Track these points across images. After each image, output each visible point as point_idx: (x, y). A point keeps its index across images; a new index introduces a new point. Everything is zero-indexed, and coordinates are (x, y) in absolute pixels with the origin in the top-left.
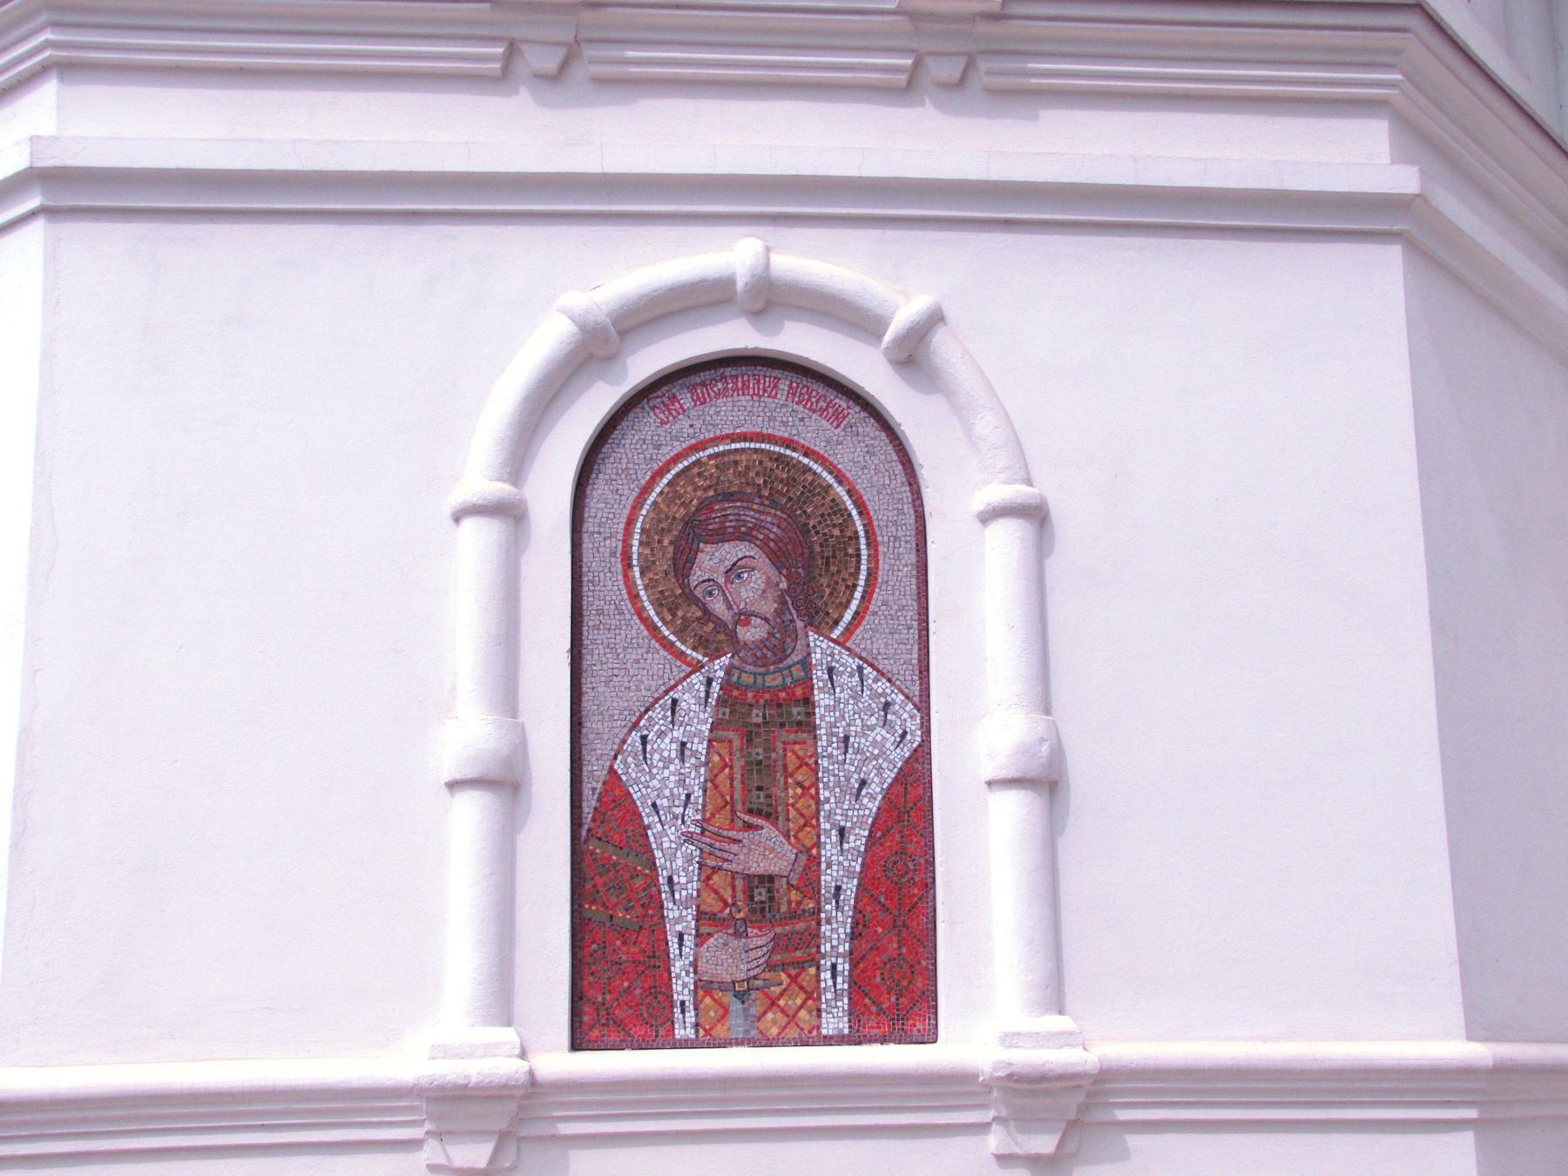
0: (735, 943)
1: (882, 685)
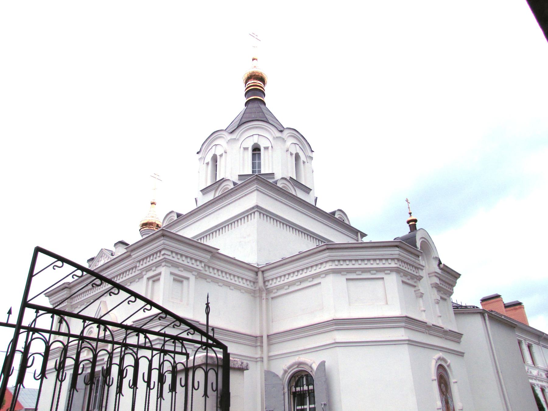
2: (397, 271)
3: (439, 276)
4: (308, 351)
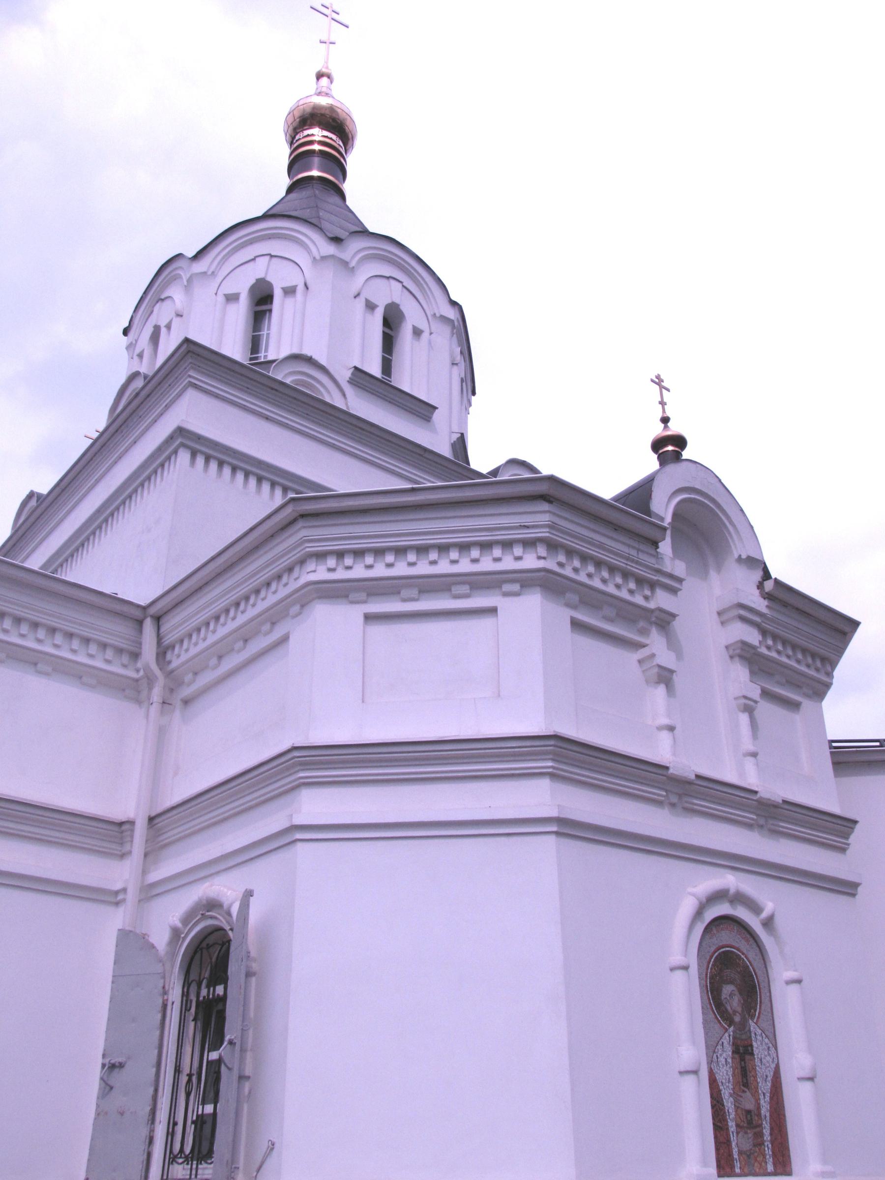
0: (745, 1136)
1: (766, 1040)
2: (549, 584)
3: (757, 619)
4: (231, 863)
